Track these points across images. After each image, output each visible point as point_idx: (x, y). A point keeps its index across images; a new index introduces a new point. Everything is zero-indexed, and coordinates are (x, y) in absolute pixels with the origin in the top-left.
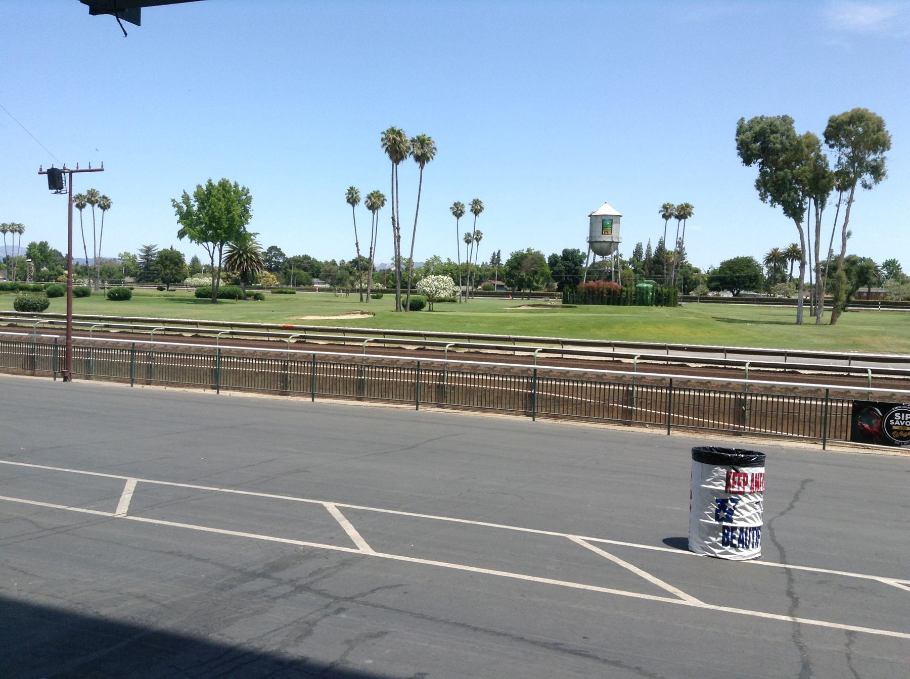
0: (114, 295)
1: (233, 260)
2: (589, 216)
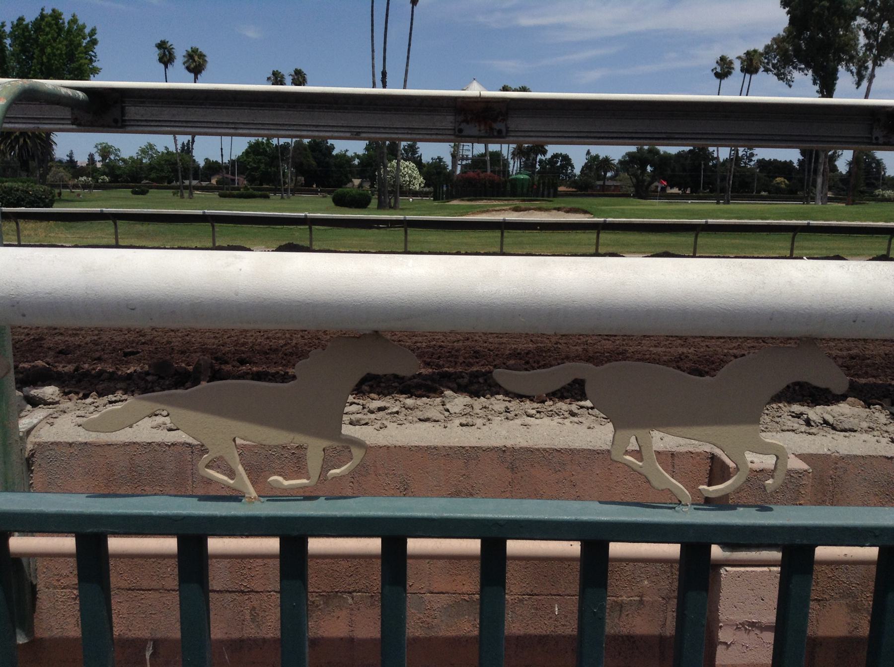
1: (13, 137)
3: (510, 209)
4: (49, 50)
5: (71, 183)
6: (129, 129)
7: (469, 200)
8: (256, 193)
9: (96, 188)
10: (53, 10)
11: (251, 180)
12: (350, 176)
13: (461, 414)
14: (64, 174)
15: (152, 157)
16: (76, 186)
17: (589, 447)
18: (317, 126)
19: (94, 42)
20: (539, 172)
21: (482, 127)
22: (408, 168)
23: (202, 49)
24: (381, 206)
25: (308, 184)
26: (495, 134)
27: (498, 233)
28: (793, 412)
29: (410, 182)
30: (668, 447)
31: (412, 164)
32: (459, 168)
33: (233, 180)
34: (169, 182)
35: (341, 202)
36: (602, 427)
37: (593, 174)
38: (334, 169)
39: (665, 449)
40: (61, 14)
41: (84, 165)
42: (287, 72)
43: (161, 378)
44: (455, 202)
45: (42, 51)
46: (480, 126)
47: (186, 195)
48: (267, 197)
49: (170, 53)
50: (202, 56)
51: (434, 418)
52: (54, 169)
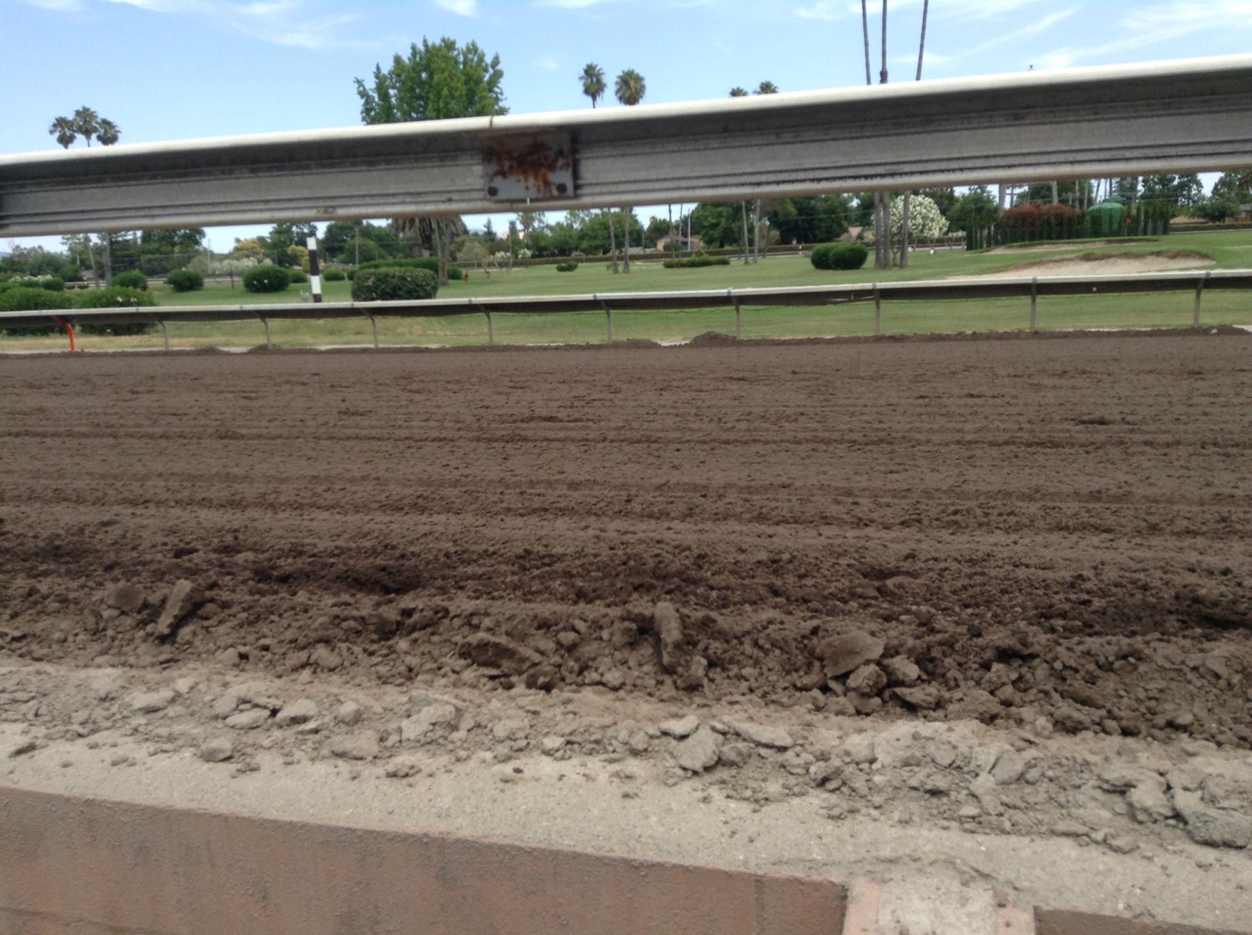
0: (260, 281)
3: (1077, 258)
4: (445, 92)
5: (485, 261)
6: (13, 229)
7: (1020, 247)
8: (712, 258)
9: (516, 264)
10: (443, 40)
11: (709, 242)
12: (845, 223)
13: (419, 741)
14: (479, 249)
15: (583, 220)
16: (491, 265)
17: (589, 851)
18: (267, 202)
19: (498, 75)
20: (1143, 197)
21: (531, 181)
22: (924, 206)
23: (639, 71)
24: (882, 264)
25: (784, 241)
26: (555, 192)
27: (1026, 300)
28: (1107, 782)
29: (924, 226)
30: (752, 864)
31: (928, 200)
32: (1008, 199)
33: (685, 243)
34: (606, 252)
35: (822, 262)
36: (668, 790)
37: (1233, 194)
38: (822, 216)
39: (742, 869)
40: (453, 43)
41: (505, 237)
42: (752, 85)
43: (123, 613)
44: (999, 251)
45: (439, 94)
46: (526, 179)
47: (621, 268)
48: (725, 263)
49: (599, 81)
50: (639, 79)
51: (355, 753)
52: (467, 244)
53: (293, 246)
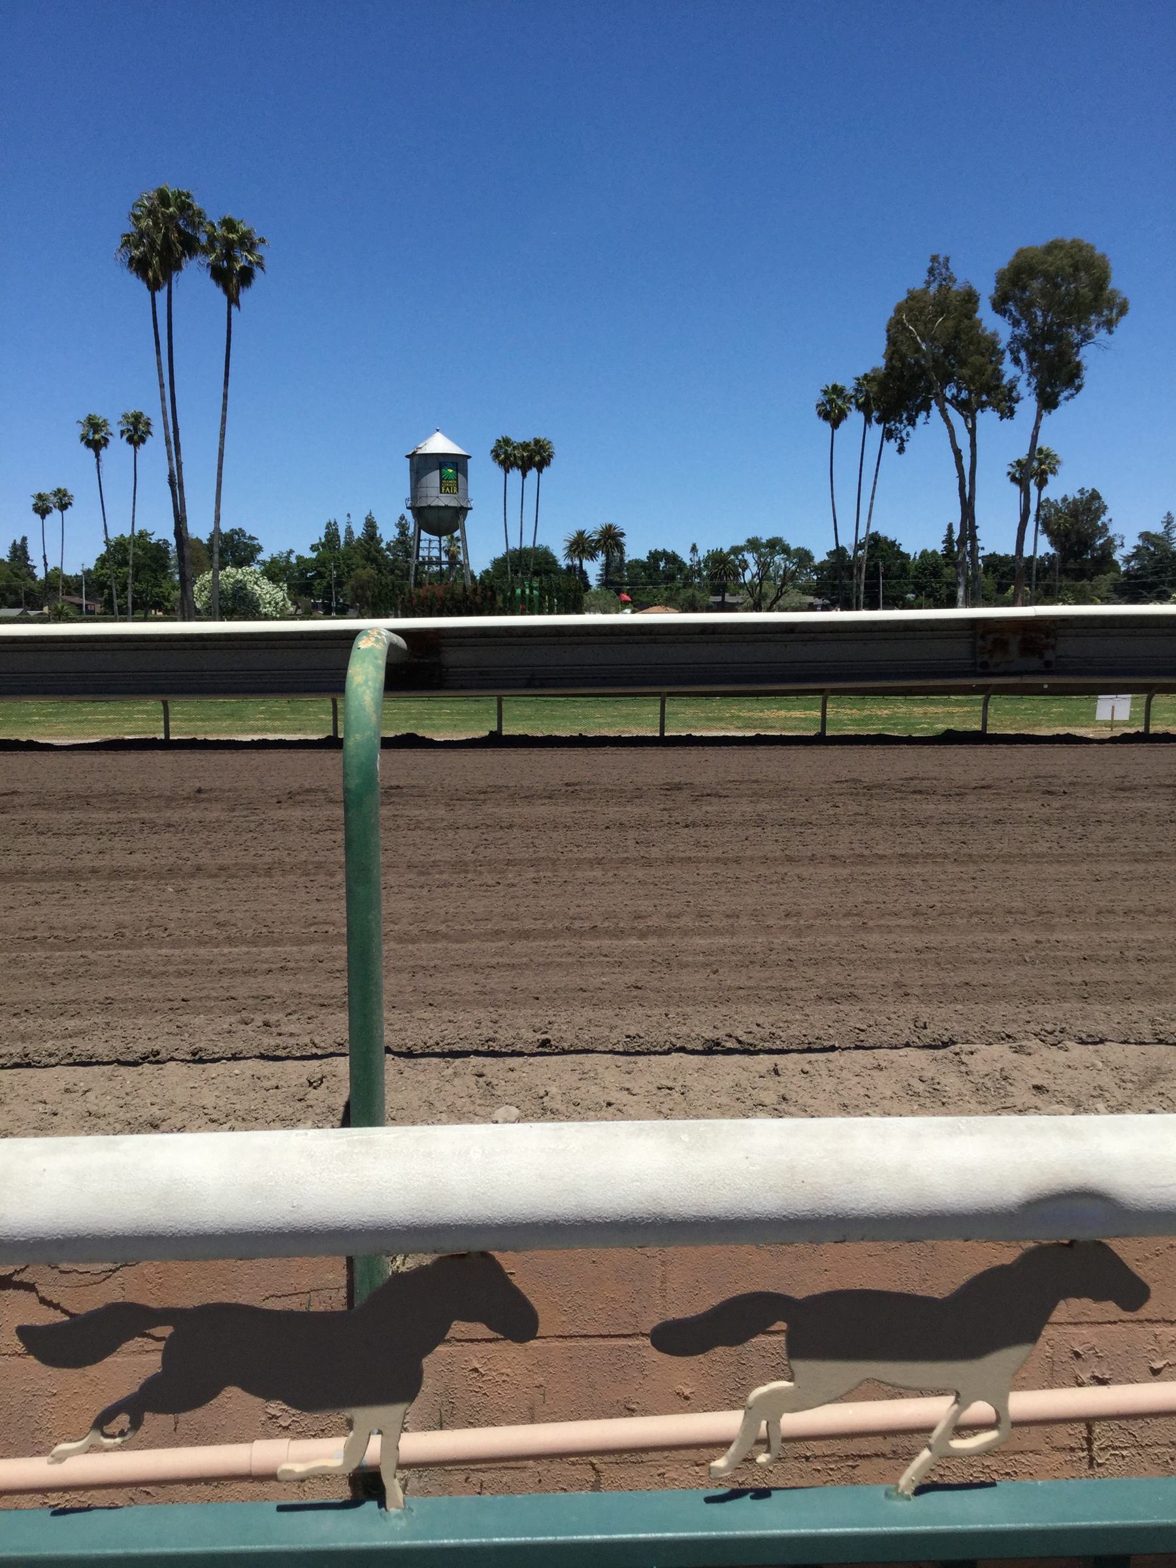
2: (407, 456)
53: (221, 573)
